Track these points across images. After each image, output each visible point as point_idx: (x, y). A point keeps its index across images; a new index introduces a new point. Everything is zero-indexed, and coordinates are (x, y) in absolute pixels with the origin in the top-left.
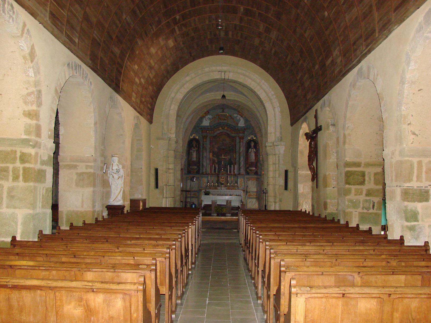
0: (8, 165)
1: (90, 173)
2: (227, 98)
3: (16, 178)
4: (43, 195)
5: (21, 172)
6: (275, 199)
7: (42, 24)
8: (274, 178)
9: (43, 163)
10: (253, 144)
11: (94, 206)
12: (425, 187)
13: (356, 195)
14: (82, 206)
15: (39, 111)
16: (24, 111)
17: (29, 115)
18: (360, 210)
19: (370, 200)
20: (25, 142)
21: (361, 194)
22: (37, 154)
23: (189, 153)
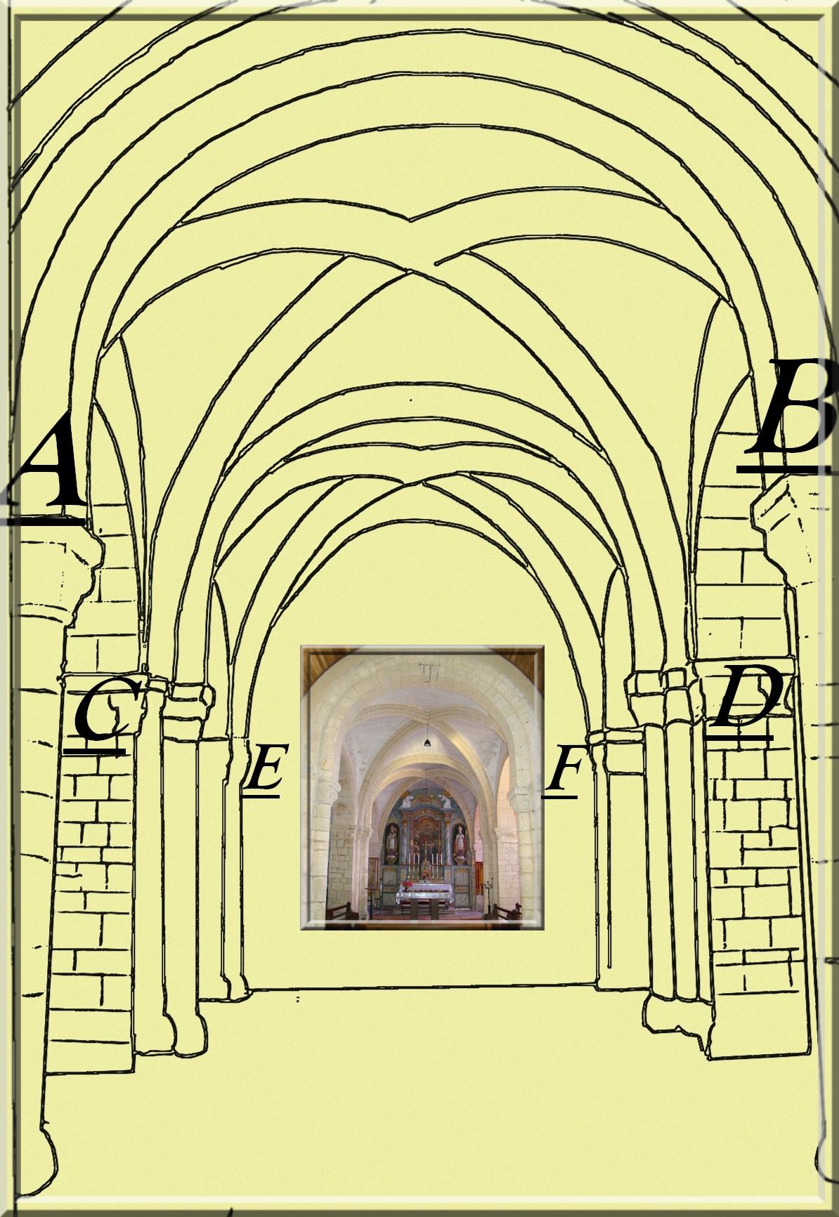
10: (460, 829)
23: (386, 841)
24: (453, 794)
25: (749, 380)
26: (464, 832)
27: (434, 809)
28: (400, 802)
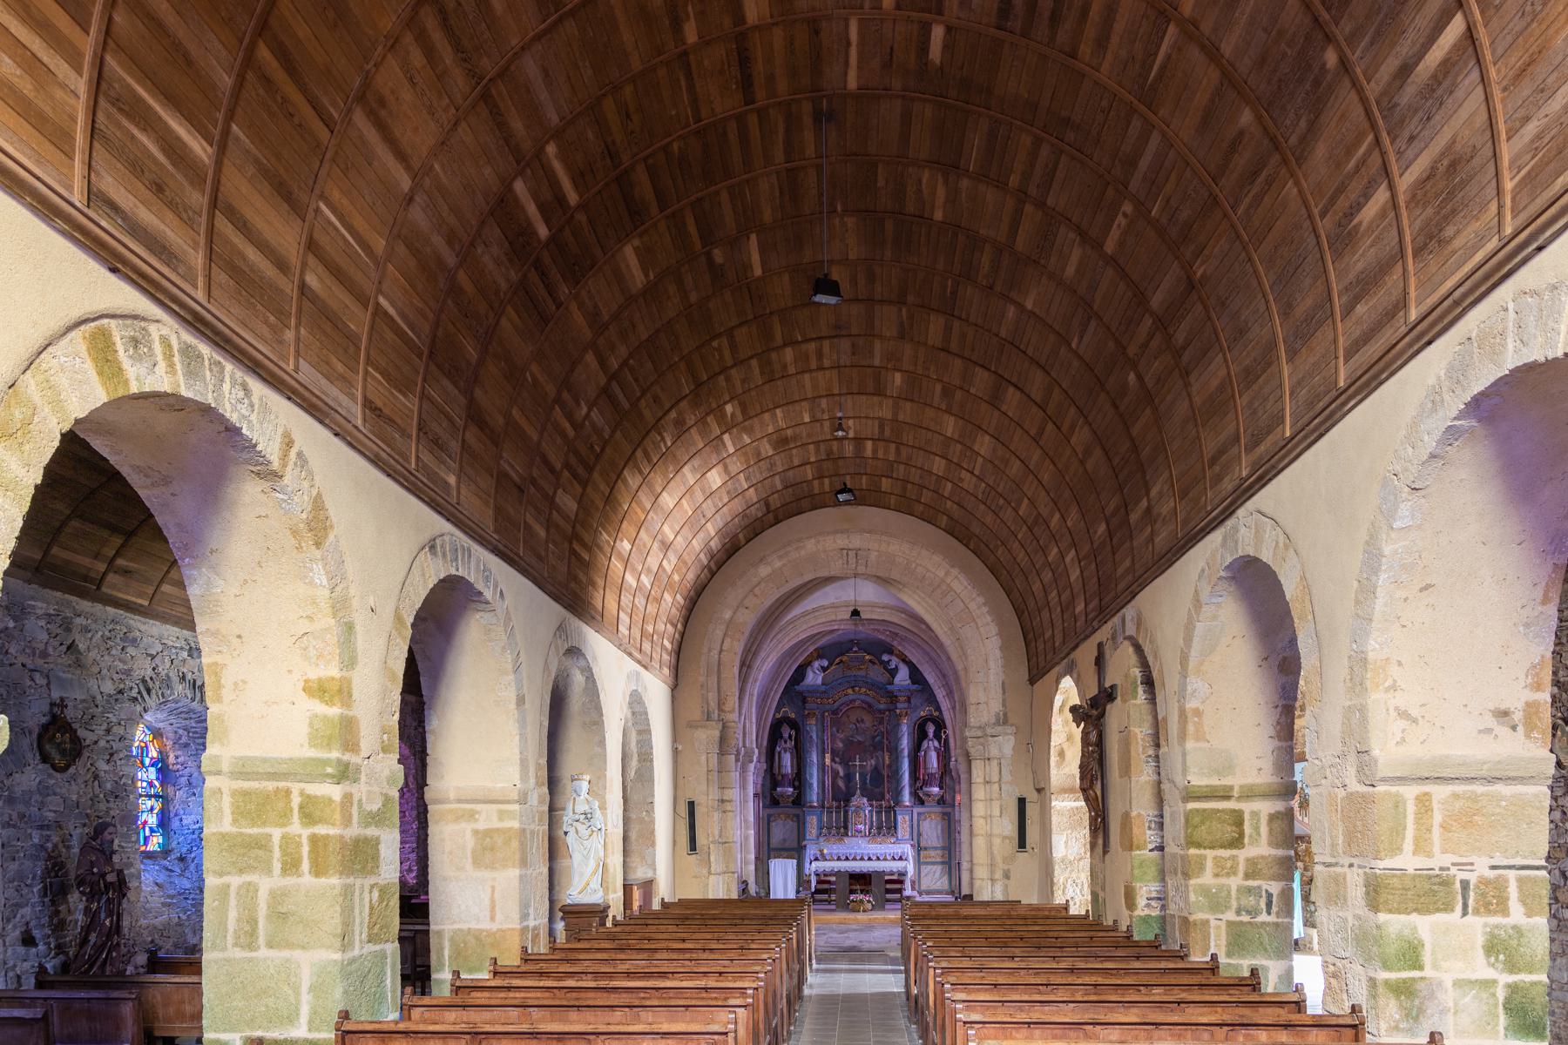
0: (267, 830)
1: (510, 829)
2: (863, 616)
3: (291, 866)
4: (372, 908)
5: (305, 849)
6: (992, 872)
7: (344, 439)
8: (988, 817)
9: (375, 819)
10: (931, 729)
11: (524, 917)
12: (1441, 869)
13: (1217, 875)
14: (492, 918)
15: (349, 681)
16: (306, 681)
17: (318, 690)
18: (1231, 916)
19: (1259, 887)
20: (310, 770)
21: (1233, 871)
22: (348, 797)
23: (771, 755)
26: (937, 736)
27: (873, 686)
28: (800, 674)
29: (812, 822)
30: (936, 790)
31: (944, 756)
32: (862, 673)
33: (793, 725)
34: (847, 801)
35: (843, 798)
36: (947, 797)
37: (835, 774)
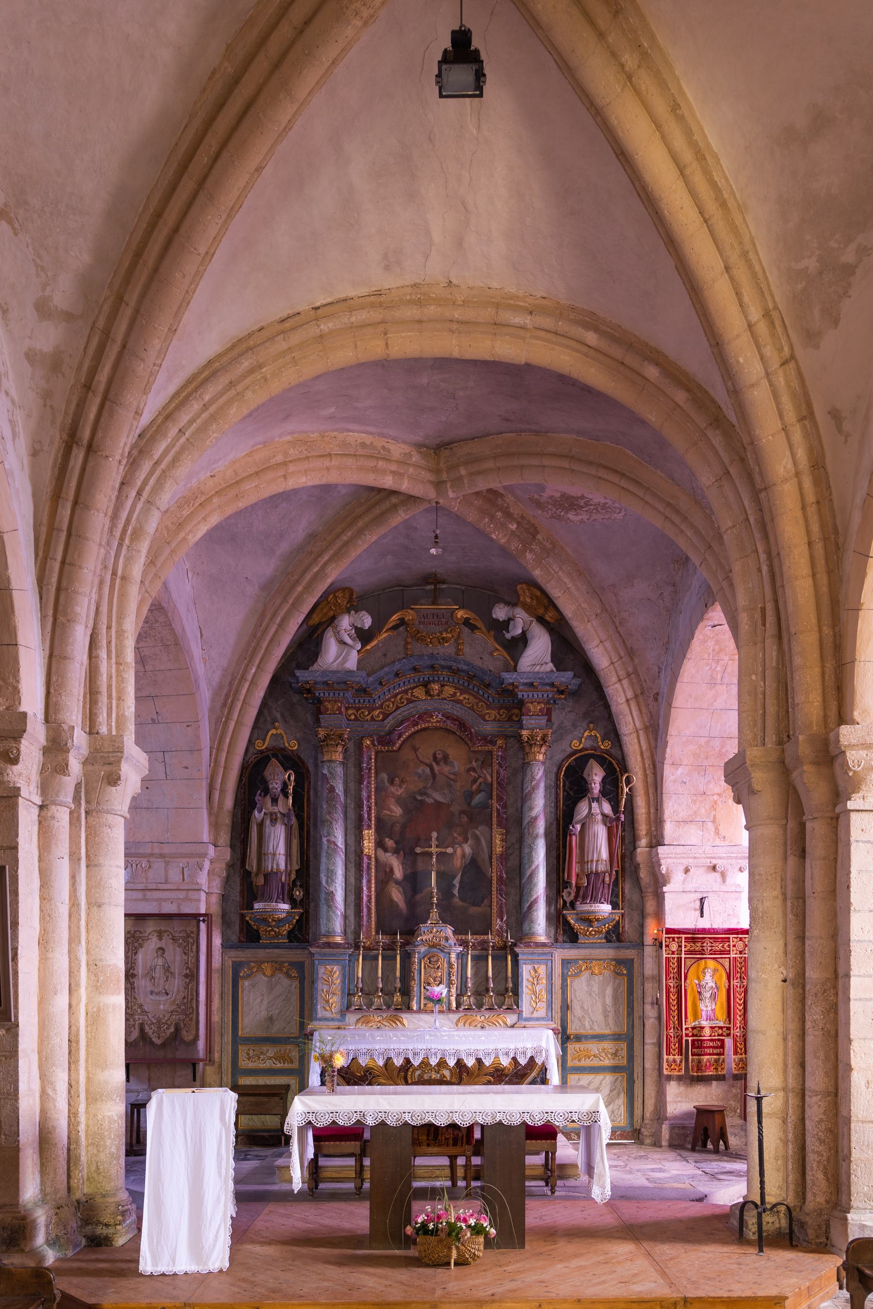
10: (596, 777)
23: (242, 832)
24: (571, 603)
25: (759, 1203)
26: (611, 790)
27: (472, 680)
28: (308, 645)
29: (331, 979)
30: (605, 908)
31: (623, 831)
32: (448, 649)
33: (290, 761)
34: (410, 933)
35: (398, 926)
36: (628, 928)
37: (385, 876)
